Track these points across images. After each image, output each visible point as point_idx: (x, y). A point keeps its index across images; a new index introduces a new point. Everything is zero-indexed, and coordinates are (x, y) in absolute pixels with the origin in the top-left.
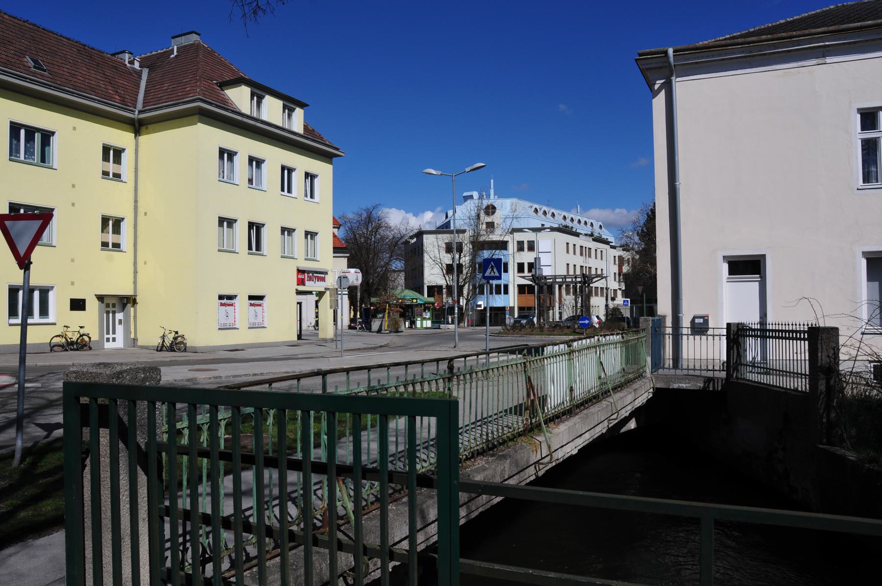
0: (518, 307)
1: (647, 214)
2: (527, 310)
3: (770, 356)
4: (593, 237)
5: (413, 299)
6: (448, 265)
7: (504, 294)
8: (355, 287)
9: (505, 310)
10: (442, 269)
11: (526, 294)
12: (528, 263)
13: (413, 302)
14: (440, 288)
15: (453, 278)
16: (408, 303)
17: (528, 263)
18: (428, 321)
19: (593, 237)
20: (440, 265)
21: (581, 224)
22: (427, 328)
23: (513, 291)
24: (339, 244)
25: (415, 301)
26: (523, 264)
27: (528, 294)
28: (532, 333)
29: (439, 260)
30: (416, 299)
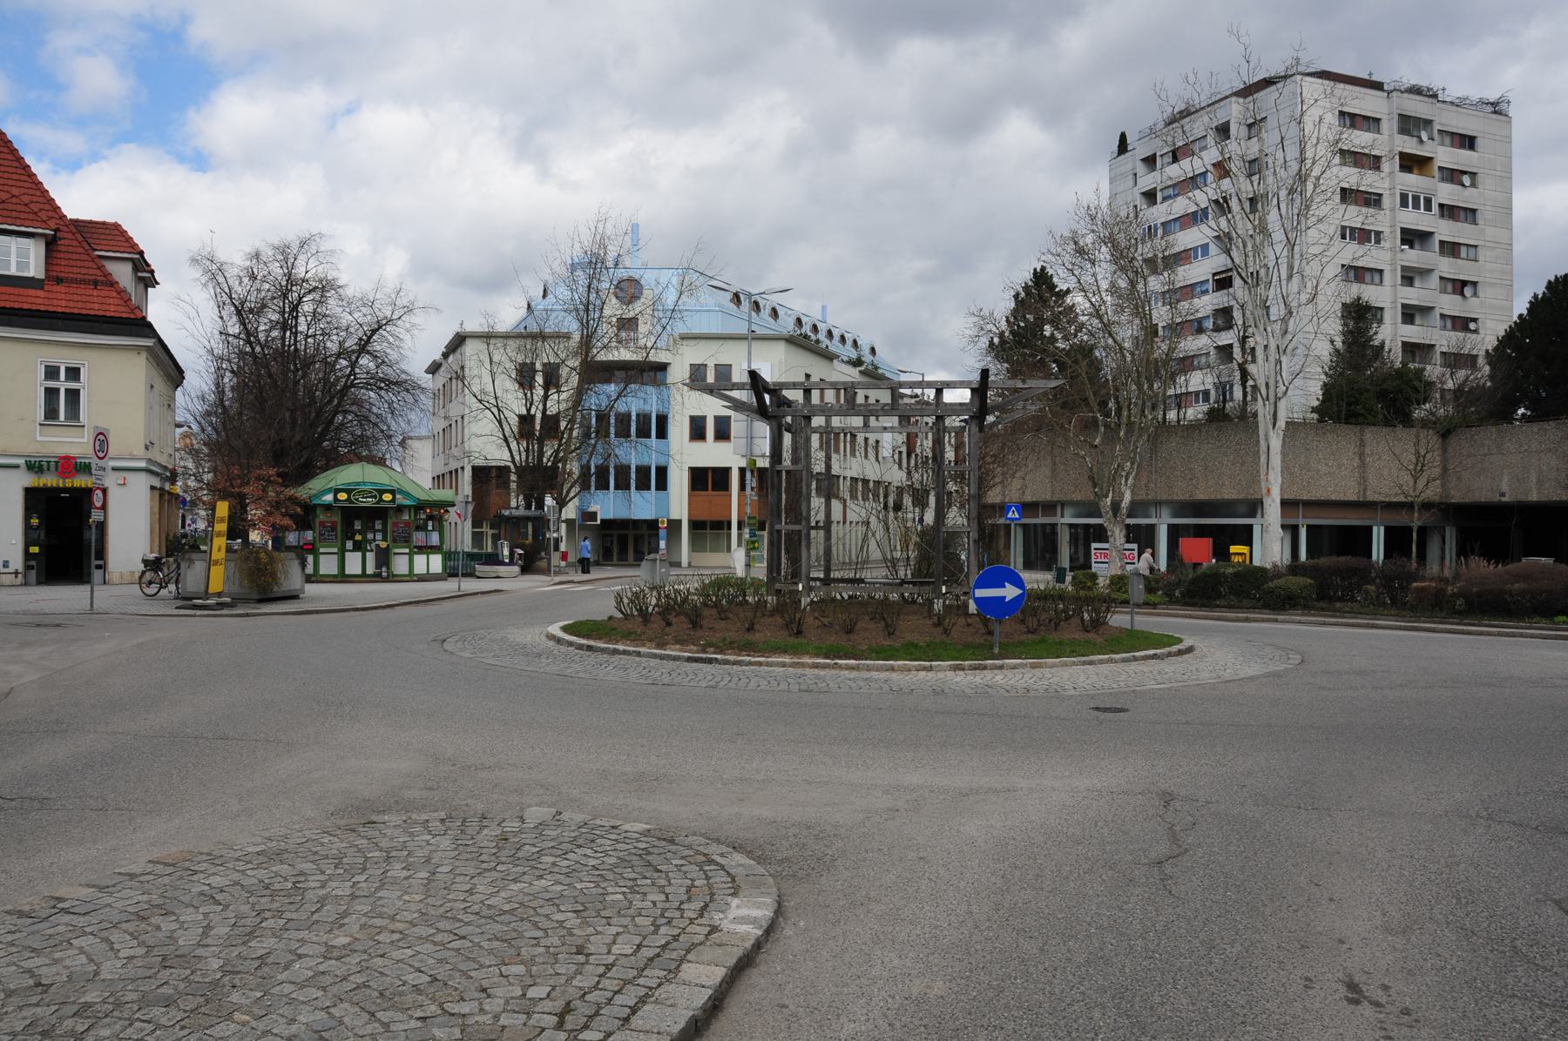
0: (689, 521)
1: (1016, 296)
2: (711, 529)
3: (1136, 623)
4: (862, 368)
5: (382, 492)
6: (521, 417)
7: (657, 488)
8: (574, 520)
9: (658, 528)
10: (500, 422)
11: (710, 492)
12: (715, 417)
13: (381, 500)
14: (502, 471)
15: (528, 447)
16: (369, 502)
17: (715, 417)
18: (431, 556)
19: (862, 368)
20: (495, 410)
21: (833, 341)
22: (422, 578)
23: (679, 482)
24: (121, 309)
25: (387, 497)
26: (703, 418)
27: (713, 490)
28: (750, 637)
29: (493, 401)
30: (393, 492)
